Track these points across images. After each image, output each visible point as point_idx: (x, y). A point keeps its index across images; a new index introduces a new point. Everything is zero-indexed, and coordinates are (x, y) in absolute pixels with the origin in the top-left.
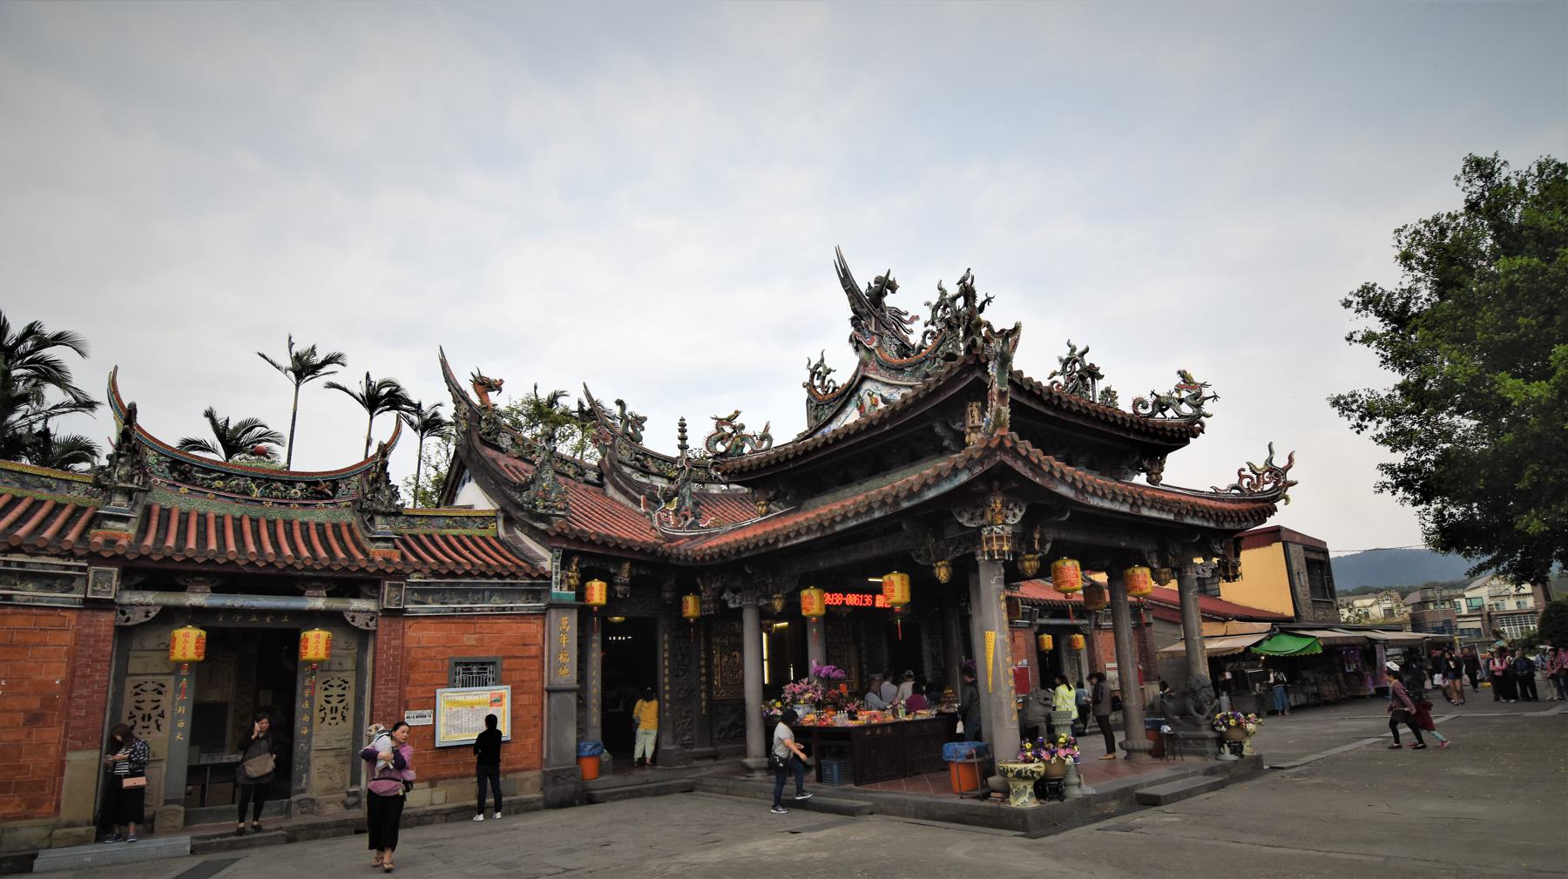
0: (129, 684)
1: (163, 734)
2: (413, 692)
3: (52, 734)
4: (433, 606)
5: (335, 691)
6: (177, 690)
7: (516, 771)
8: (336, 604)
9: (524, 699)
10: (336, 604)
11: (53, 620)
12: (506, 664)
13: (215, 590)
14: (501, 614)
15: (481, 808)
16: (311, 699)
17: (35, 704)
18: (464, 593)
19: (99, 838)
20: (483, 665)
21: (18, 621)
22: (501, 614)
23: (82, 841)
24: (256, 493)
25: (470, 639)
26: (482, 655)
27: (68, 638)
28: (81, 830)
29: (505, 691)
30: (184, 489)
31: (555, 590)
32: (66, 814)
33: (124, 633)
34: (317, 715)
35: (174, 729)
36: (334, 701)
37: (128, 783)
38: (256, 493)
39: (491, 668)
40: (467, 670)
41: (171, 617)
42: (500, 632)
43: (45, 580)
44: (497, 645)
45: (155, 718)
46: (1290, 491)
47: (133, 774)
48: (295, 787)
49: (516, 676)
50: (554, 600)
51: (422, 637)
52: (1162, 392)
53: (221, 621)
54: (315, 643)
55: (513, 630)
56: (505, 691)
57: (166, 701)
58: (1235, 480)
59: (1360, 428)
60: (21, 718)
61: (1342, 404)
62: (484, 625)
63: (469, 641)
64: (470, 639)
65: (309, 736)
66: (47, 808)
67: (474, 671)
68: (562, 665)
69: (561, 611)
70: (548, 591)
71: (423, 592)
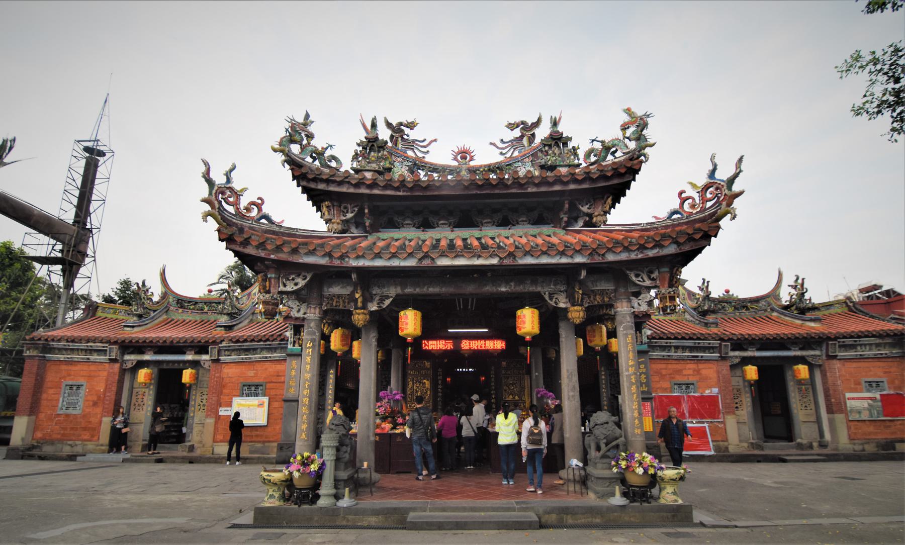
0: (135, 391)
1: (144, 412)
2: (224, 398)
3: (98, 410)
4: (234, 357)
5: (205, 397)
6: (149, 394)
7: (269, 442)
8: (197, 357)
9: (276, 405)
10: (197, 357)
11: (101, 367)
12: (268, 386)
13: (155, 353)
14: (266, 360)
15: (229, 458)
16: (195, 400)
17: (95, 399)
18: (247, 350)
19: (109, 452)
20: (257, 386)
21: (93, 368)
22: (266, 360)
23: (103, 452)
24: (206, 309)
25: (251, 373)
26: (256, 381)
27: (105, 373)
28: (103, 448)
29: (266, 400)
30: (181, 310)
31: (290, 346)
32: (101, 442)
33: (123, 371)
34: (197, 408)
35: (147, 411)
36: (204, 401)
37: (124, 431)
38: (206, 309)
39: (691, 386)
40: (871, 386)
41: (141, 364)
42: (266, 369)
43: (99, 351)
44: (264, 376)
45: (141, 406)
46: (737, 203)
47: (125, 427)
48: (187, 439)
49: (273, 393)
50: (289, 352)
51: (229, 372)
52: (608, 138)
53: (165, 366)
54: (187, 376)
55: (273, 368)
56: (266, 400)
57: (145, 398)
58: (676, 205)
59: (359, 145)
60: (91, 403)
61: (385, 118)
62: (258, 366)
63: (251, 374)
64: (251, 373)
65: (193, 417)
66: (96, 438)
67: (251, 389)
68: (291, 387)
69: (292, 358)
70: (286, 348)
71: (230, 351)
